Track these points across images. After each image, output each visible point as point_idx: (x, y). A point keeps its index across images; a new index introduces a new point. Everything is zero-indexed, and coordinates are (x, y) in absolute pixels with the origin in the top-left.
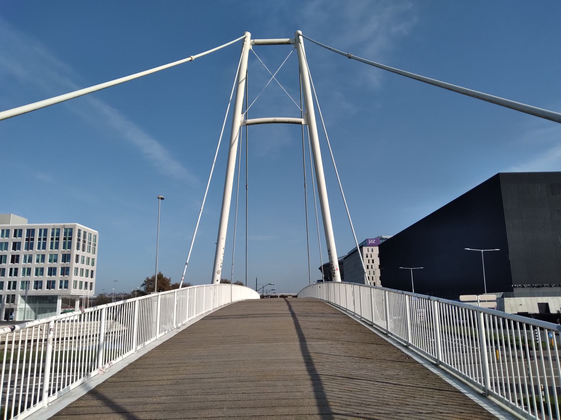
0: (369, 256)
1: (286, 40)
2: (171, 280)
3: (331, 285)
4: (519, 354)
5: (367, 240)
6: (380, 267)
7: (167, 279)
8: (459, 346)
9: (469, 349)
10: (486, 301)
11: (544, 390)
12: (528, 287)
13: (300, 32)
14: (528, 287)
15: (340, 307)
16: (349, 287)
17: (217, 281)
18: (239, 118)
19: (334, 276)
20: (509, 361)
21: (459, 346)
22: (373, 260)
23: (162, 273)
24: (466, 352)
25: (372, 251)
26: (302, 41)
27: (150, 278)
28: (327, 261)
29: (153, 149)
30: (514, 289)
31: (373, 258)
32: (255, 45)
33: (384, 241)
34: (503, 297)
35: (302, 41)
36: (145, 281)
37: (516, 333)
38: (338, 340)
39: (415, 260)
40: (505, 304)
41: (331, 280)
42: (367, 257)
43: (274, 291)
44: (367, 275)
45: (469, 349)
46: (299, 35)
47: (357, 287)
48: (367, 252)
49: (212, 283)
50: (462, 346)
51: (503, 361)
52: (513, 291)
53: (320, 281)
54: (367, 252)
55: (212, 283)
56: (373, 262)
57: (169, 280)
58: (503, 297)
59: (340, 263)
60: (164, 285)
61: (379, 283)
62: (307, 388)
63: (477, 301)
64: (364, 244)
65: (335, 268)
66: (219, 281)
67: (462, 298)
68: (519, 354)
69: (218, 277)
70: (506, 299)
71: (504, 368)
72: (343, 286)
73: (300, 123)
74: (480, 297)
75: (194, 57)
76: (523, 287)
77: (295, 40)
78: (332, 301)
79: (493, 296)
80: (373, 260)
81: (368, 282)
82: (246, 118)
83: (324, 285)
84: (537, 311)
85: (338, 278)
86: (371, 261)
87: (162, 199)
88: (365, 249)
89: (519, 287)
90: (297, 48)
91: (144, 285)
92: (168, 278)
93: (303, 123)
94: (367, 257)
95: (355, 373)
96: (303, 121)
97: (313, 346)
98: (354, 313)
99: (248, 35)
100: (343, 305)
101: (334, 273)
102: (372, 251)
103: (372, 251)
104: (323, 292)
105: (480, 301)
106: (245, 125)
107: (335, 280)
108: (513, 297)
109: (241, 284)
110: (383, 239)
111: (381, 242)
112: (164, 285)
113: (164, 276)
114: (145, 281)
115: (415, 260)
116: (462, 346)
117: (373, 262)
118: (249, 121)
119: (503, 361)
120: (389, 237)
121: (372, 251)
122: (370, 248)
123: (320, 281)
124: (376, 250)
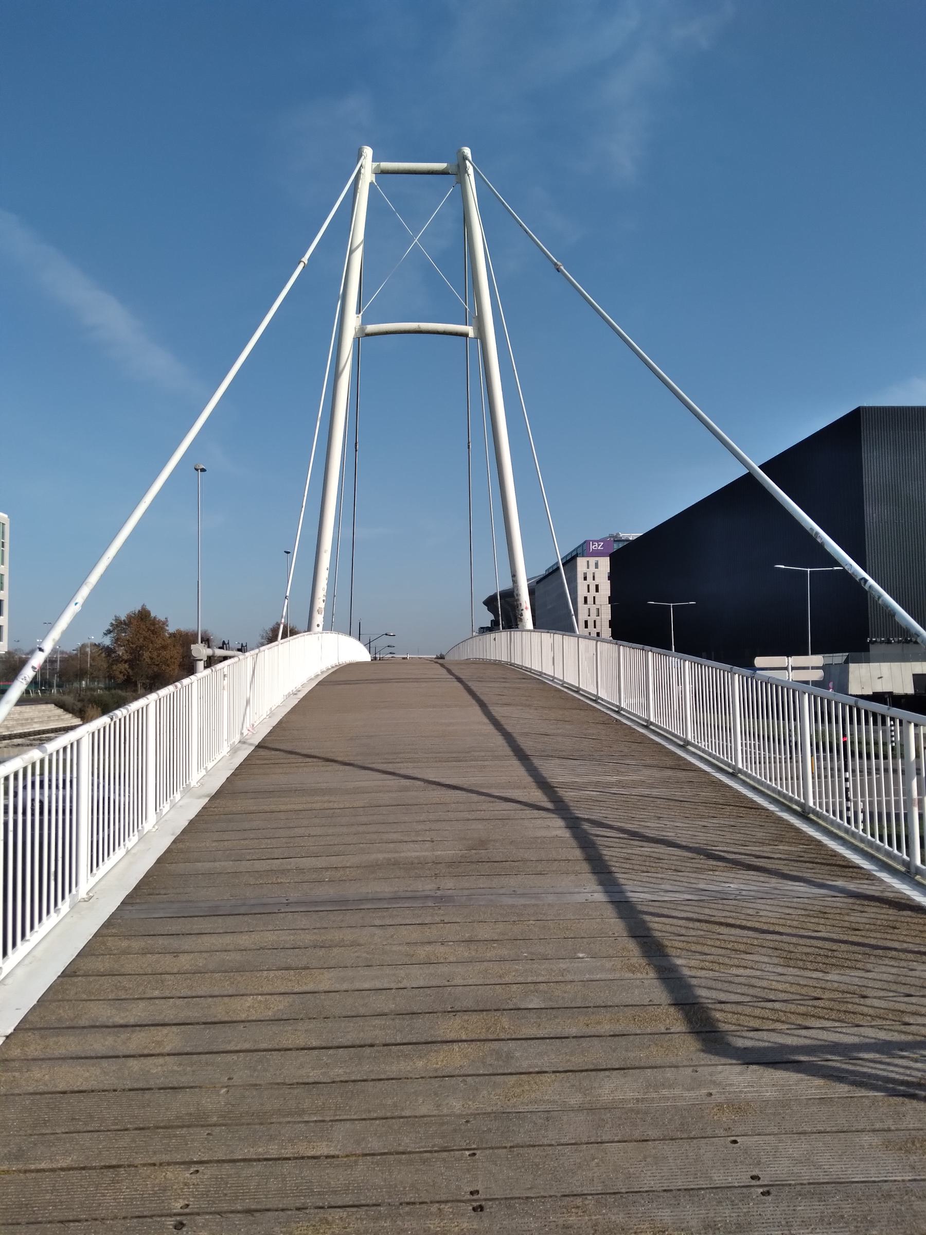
0: (590, 577)
1: (441, 166)
2: (170, 623)
3: (516, 635)
4: (861, 765)
5: (586, 543)
6: (611, 600)
7: (159, 621)
8: (755, 753)
9: (769, 758)
10: (806, 667)
11: (863, 812)
12: (899, 642)
13: (467, 151)
14: (899, 642)
15: (530, 670)
16: (546, 638)
17: (318, 626)
18: (353, 322)
19: (521, 620)
20: (833, 776)
21: (755, 753)
22: (597, 586)
23: (148, 607)
24: (765, 763)
25: (597, 566)
26: (471, 171)
27: (123, 618)
28: (508, 585)
29: (108, 316)
30: (871, 647)
31: (597, 582)
32: (381, 173)
33: (621, 545)
34: (847, 662)
35: (471, 171)
36: (112, 625)
37: (867, 731)
38: (529, 706)
39: (694, 586)
40: (851, 676)
41: (517, 626)
42: (585, 579)
43: (391, 650)
44: (583, 616)
45: (769, 758)
46: (465, 158)
47: (558, 637)
48: (585, 569)
49: (309, 629)
50: (760, 754)
51: (826, 777)
52: (869, 651)
53: (484, 630)
54: (585, 569)
55: (309, 629)
56: (597, 590)
57: (165, 623)
58: (847, 662)
59: (532, 592)
60: (154, 632)
61: (607, 632)
62: (500, 740)
63: (786, 669)
64: (579, 551)
65: (524, 606)
66: (321, 626)
67: (759, 661)
68: (861, 765)
69: (319, 619)
70: (852, 666)
71: (820, 787)
72: (536, 636)
73: (465, 335)
74: (793, 661)
75: (305, 259)
76: (889, 642)
77: (458, 166)
78: (518, 662)
79: (818, 660)
80: (597, 586)
81: (579, 629)
82: (365, 322)
83: (502, 636)
84: (910, 690)
85: (529, 624)
86: (593, 588)
87: (203, 470)
88: (581, 562)
89: (881, 642)
90: (462, 183)
91: (109, 632)
92: (163, 619)
93: (471, 334)
94: (585, 579)
95: (549, 732)
96: (470, 330)
97: (497, 711)
98: (553, 677)
99: (368, 152)
100: (536, 667)
101: (522, 615)
102: (597, 566)
103: (597, 566)
104: (499, 646)
105: (793, 668)
106: (362, 336)
107: (523, 626)
108: (868, 661)
109: (290, 632)
110: (621, 541)
111: (616, 547)
112: (154, 632)
113: (153, 615)
114: (112, 625)
115: (694, 586)
116: (760, 754)
117: (597, 590)
118: (371, 328)
119: (826, 777)
120: (633, 536)
121: (597, 566)
122: (592, 560)
123: (484, 630)
124: (605, 564)
